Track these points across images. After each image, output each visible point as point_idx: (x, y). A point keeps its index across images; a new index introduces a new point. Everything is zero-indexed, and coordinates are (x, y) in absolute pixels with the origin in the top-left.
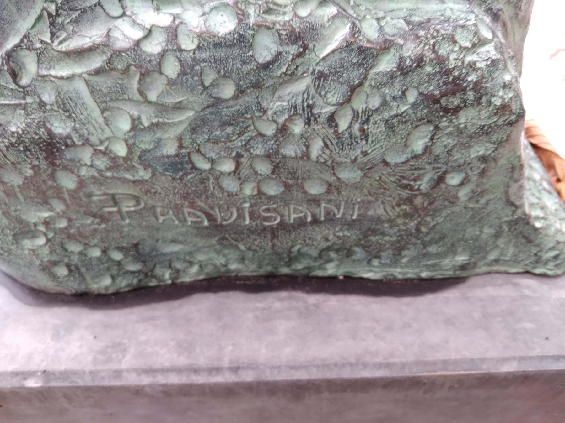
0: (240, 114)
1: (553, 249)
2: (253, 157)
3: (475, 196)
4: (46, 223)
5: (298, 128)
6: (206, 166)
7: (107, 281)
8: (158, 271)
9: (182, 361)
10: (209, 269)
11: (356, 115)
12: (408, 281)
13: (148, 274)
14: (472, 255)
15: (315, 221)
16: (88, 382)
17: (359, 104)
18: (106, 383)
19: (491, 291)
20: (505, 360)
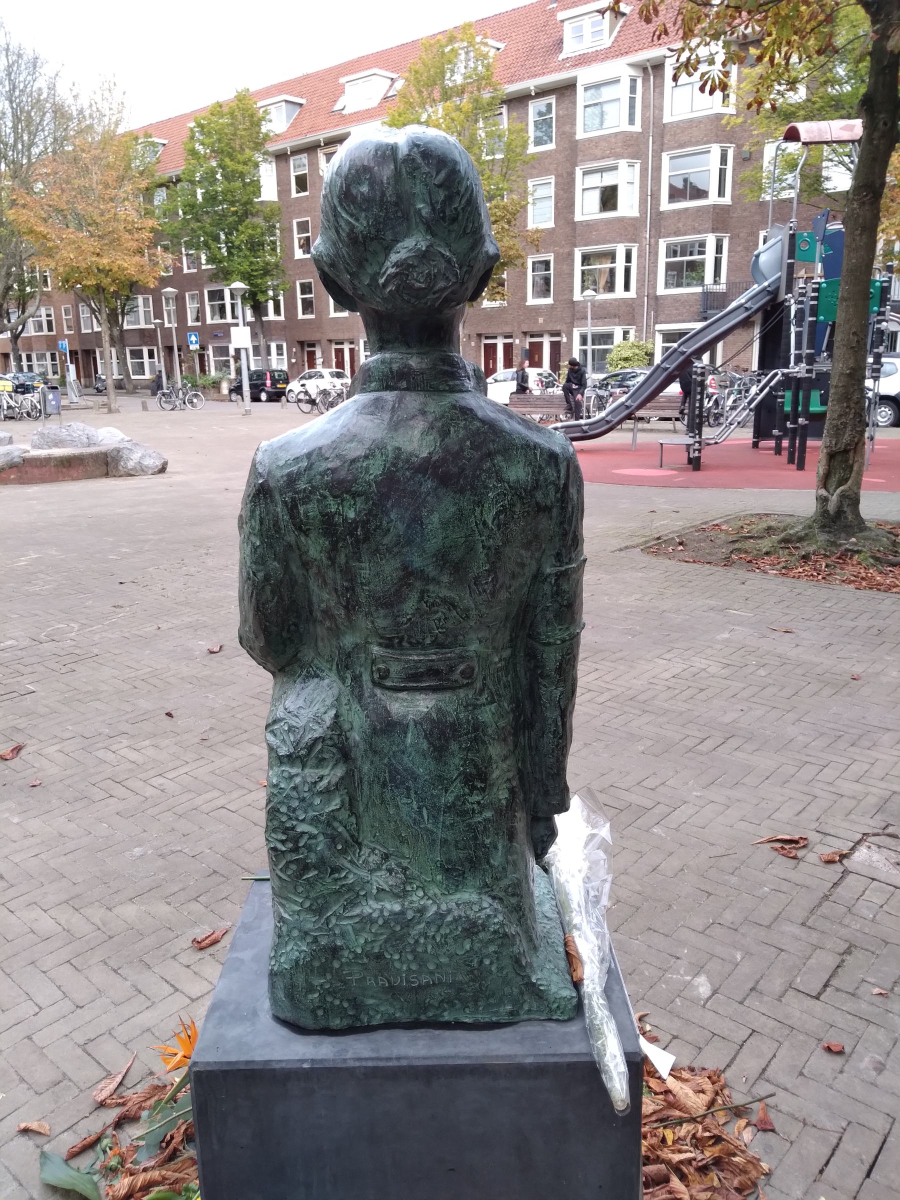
0: (402, 936)
1: (554, 1002)
2: (406, 952)
3: (501, 969)
4: (321, 985)
5: (422, 941)
6: (389, 957)
7: (338, 1022)
8: (362, 1016)
9: (374, 1055)
10: (386, 1016)
11: (442, 936)
12: (487, 1023)
13: (356, 1017)
14: (513, 1005)
15: (434, 984)
16: (331, 1065)
17: (442, 932)
18: (339, 1066)
19: (529, 1028)
20: (527, 1056)
